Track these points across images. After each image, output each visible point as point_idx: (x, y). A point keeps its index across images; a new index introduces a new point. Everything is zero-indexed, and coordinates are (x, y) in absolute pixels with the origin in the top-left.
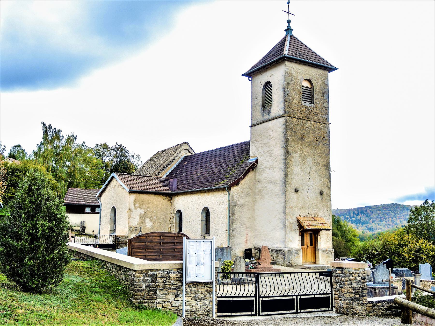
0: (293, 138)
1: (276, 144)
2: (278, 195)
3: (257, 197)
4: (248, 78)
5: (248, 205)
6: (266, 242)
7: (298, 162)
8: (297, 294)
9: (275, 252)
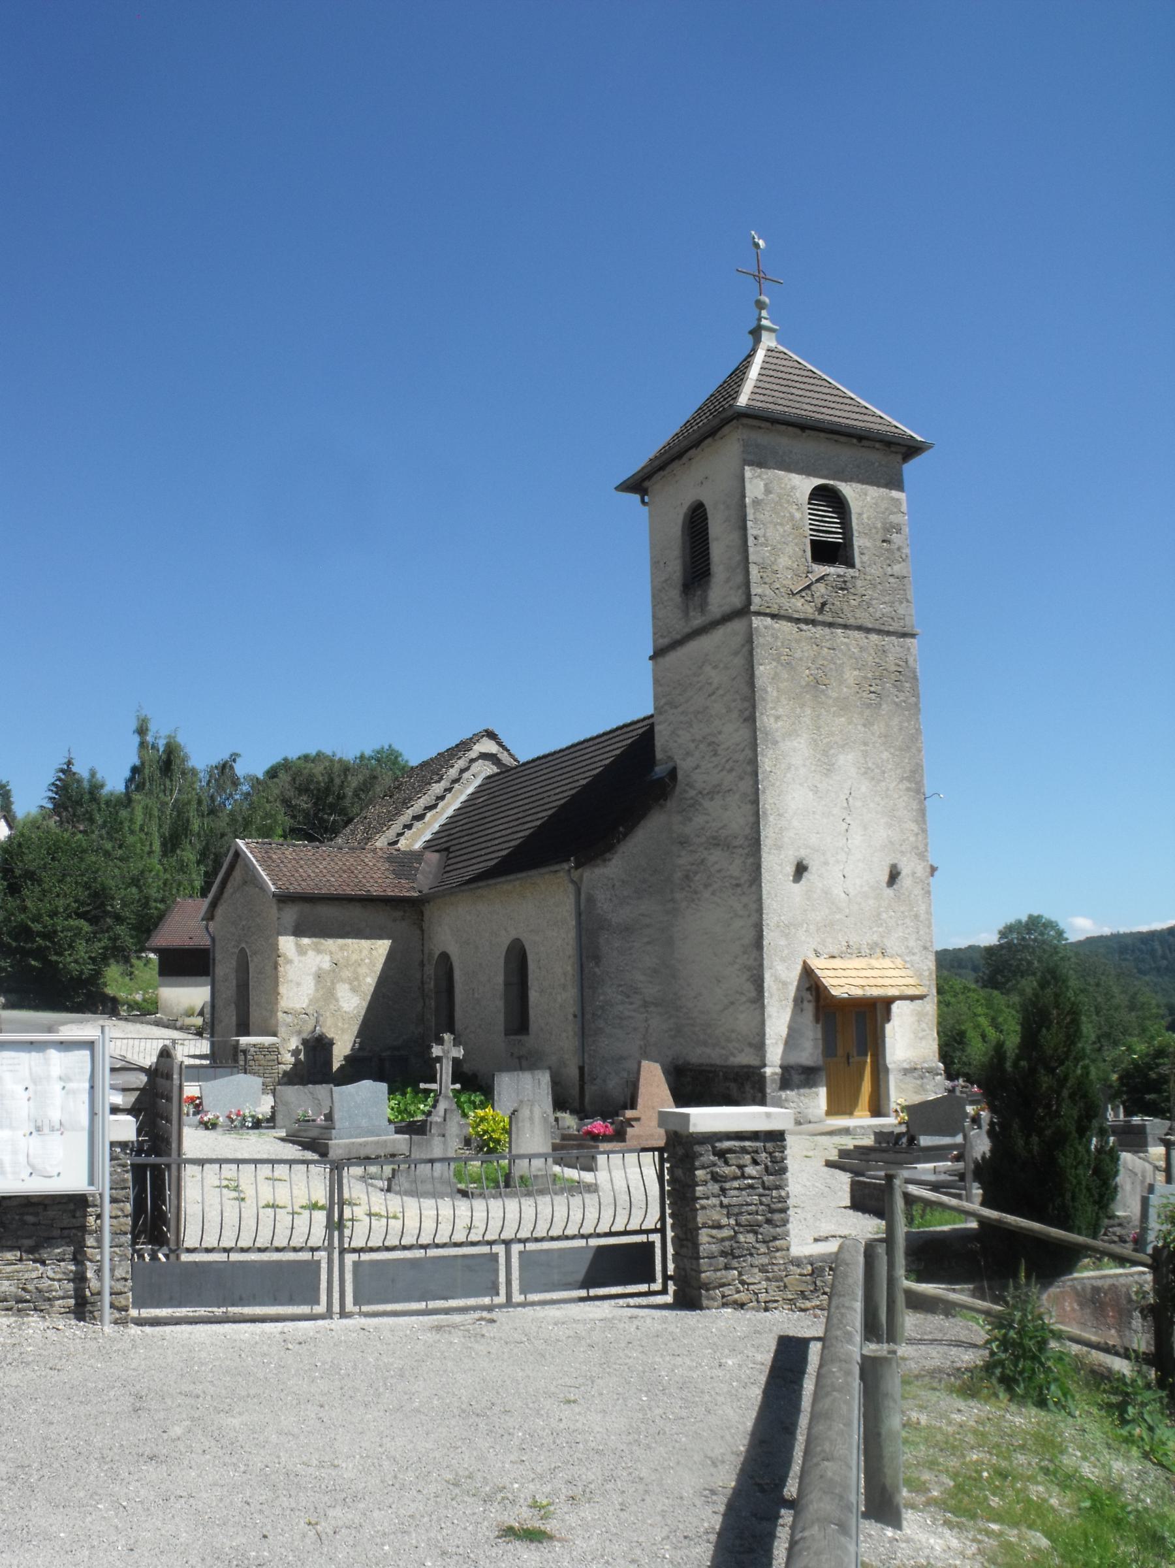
0: (782, 686)
1: (729, 710)
2: (738, 885)
3: (678, 896)
4: (637, 497)
5: (648, 926)
6: (708, 1051)
7: (802, 771)
8: (507, 1235)
9: (735, 1080)
